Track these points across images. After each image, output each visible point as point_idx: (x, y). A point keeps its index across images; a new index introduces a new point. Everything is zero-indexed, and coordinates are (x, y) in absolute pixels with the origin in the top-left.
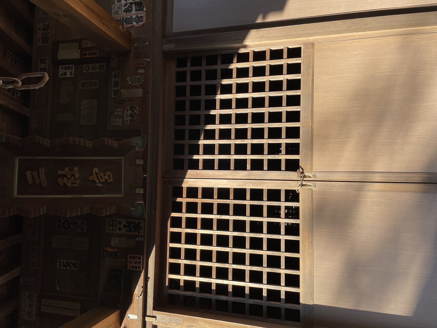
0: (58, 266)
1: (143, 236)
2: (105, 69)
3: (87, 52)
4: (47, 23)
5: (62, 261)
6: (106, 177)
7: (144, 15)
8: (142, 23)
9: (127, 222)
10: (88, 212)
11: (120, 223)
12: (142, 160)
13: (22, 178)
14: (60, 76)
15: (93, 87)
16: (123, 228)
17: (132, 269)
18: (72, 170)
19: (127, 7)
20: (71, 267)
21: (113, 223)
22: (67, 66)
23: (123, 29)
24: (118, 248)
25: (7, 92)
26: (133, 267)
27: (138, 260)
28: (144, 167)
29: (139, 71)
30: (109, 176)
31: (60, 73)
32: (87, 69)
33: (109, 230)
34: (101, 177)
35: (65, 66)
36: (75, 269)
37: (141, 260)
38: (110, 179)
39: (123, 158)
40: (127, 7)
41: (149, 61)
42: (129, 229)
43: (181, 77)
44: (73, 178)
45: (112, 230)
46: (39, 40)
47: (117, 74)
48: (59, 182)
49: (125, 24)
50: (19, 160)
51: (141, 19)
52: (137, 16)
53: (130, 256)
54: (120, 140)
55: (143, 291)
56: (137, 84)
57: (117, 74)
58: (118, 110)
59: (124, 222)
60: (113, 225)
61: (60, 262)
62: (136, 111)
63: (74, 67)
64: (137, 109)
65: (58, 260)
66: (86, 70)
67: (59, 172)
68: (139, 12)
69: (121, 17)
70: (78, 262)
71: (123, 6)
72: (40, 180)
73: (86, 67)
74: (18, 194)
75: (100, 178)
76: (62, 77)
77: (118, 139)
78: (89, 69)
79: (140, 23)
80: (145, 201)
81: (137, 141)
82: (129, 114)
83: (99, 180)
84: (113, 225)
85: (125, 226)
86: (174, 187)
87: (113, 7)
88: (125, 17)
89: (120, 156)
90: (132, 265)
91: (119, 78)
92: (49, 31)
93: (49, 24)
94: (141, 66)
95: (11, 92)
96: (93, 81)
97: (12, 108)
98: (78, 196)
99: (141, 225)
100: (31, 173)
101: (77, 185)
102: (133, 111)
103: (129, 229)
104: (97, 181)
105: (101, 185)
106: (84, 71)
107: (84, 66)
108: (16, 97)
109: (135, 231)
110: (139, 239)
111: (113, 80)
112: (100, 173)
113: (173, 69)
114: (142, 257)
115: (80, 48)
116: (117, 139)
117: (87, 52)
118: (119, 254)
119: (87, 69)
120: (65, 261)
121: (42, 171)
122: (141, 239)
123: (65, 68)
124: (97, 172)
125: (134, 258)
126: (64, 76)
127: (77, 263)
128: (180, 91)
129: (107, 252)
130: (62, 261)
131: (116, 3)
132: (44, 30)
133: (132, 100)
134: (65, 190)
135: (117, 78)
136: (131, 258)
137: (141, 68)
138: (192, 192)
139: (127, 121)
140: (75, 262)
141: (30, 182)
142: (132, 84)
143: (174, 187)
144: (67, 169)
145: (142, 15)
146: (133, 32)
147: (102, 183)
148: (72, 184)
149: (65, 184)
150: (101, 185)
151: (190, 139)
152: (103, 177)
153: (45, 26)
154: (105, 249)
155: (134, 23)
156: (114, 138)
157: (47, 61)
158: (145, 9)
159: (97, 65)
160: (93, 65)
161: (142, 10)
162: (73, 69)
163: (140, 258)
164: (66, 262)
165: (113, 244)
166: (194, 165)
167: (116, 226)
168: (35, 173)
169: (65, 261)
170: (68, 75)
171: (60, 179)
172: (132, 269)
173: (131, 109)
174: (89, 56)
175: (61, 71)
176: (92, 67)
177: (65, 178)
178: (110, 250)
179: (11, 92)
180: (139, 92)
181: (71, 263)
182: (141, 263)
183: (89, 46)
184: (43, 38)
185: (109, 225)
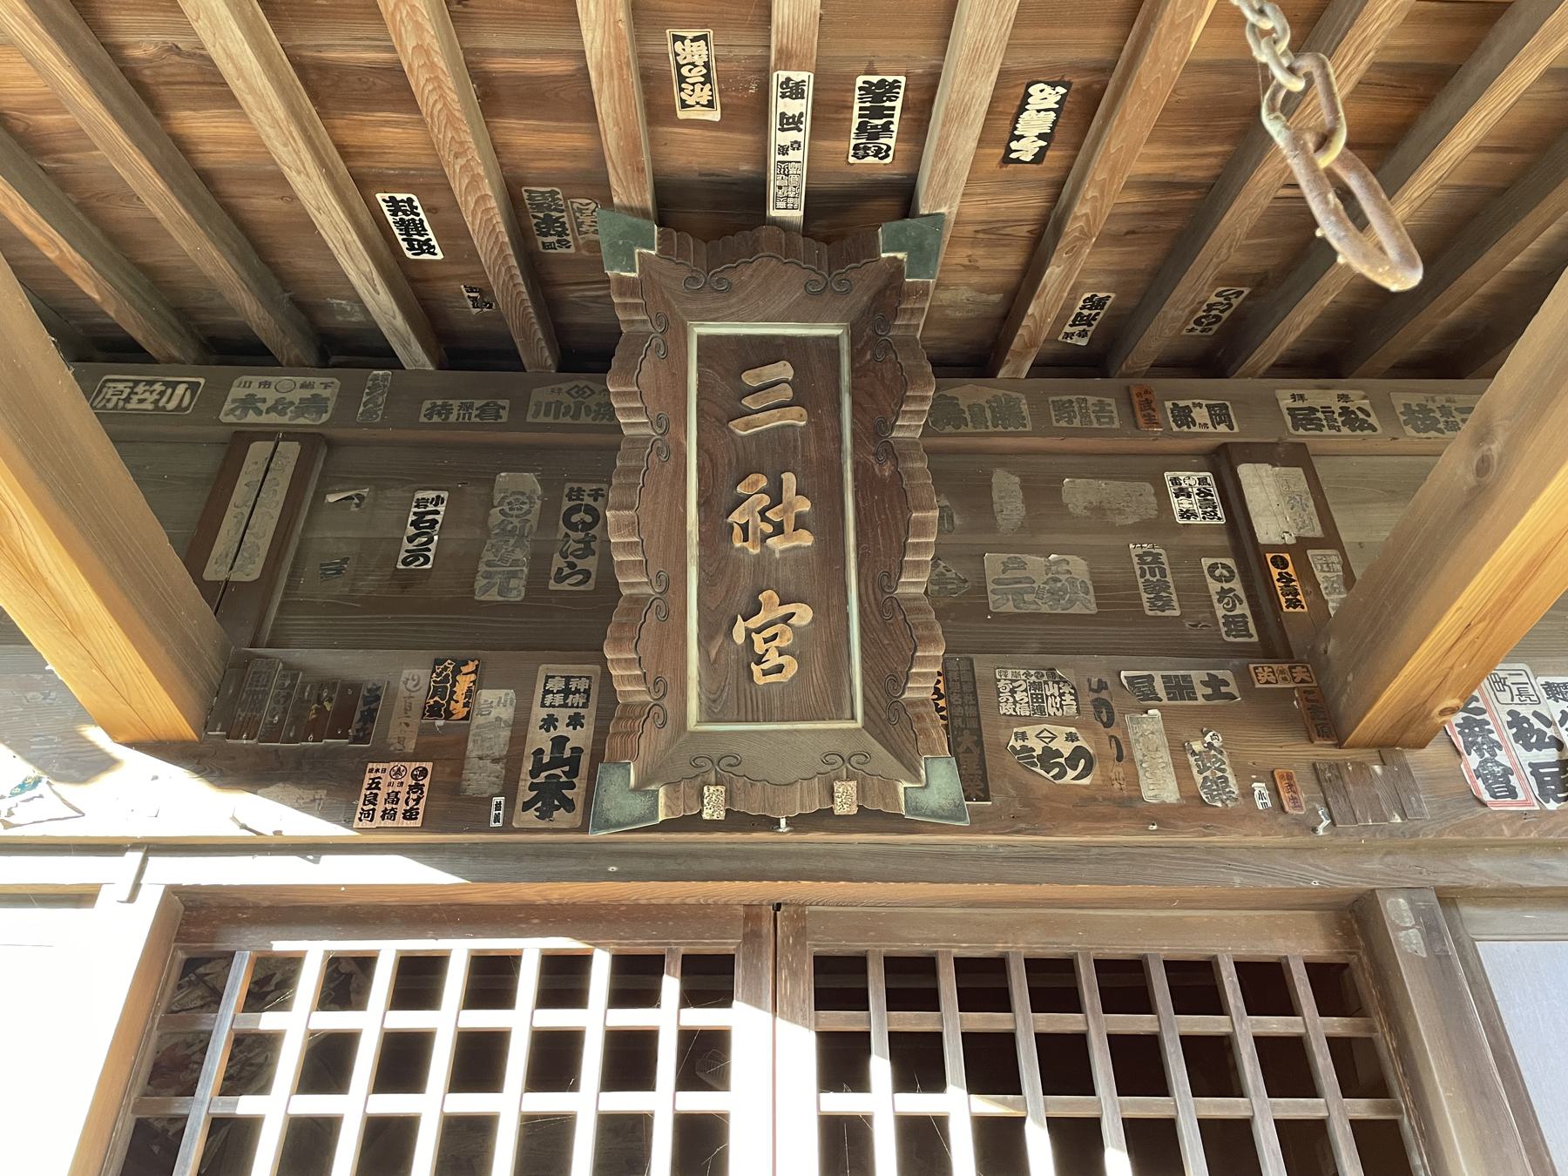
0: (419, 495)
1: (507, 828)
2: (1231, 639)
3: (1290, 569)
4: (1373, 420)
5: (441, 508)
6: (773, 659)
7: (1524, 803)
8: (1486, 797)
9: (577, 751)
10: (625, 592)
11: (575, 721)
12: (855, 810)
13: (769, 350)
14: (1168, 475)
15: (1145, 596)
16: (553, 733)
17: (367, 781)
18: (801, 522)
19: (1537, 724)
20: (411, 540)
21: (577, 691)
22: (1216, 499)
23: (1442, 713)
24: (466, 718)
25: (1088, 295)
26: (375, 784)
27: (401, 807)
28: (823, 819)
29: (1259, 787)
30: (779, 669)
31: (1182, 475)
32: (1217, 573)
33: (548, 678)
34: (774, 637)
35: (1214, 490)
36: (403, 555)
37: (400, 821)
38: (765, 673)
39: (859, 723)
40: (1537, 724)
41: (1314, 830)
42: (546, 759)
43: (1266, 985)
44: (769, 529)
45: (547, 692)
46: (1302, 397)
47: (1223, 689)
48: (753, 477)
49: (1458, 718)
50: (837, 339)
51: (1499, 788)
52: (1507, 772)
53: (424, 772)
54: (939, 710)
55: (262, 835)
56: (1199, 779)
57: (1223, 689)
58: (1068, 698)
59: (580, 737)
60: (567, 692)
61: (438, 500)
62: (1071, 774)
63: (1215, 522)
64: (1086, 781)
65: (445, 495)
66: (1213, 567)
67: (789, 480)
68: (1532, 780)
69: (1486, 702)
70: (429, 566)
71: (1537, 708)
72: (757, 412)
73: (1224, 566)
74: (704, 341)
75: (768, 633)
76: (1169, 484)
77: (942, 703)
78: (1219, 579)
79: (1480, 782)
80: (666, 826)
81: (940, 783)
82: (1054, 745)
83: (759, 631)
84: (567, 692)
85: (559, 742)
86: (730, 959)
87: (1517, 666)
88: (1486, 717)
89: (865, 713)
90: (385, 779)
91: (1206, 697)
92: (1345, 431)
93: (1375, 430)
94: (1285, 795)
95: (1086, 312)
96: (1174, 597)
97: (1030, 311)
98: (693, 551)
99: (560, 814)
100: (786, 381)
101: (738, 544)
102: (1072, 761)
103: (546, 759)
104: (755, 622)
105: (739, 635)
106: (1206, 562)
107: (1230, 562)
108: (1068, 329)
109: (532, 787)
110: (498, 806)
111: (1198, 676)
112: (789, 633)
113: (1299, 946)
114: (418, 823)
115: (1303, 544)
116: (941, 697)
117: (1290, 569)
118: (440, 723)
119: (1217, 573)
120: (439, 518)
121: (796, 418)
122: (497, 816)
123: (1203, 494)
124: (793, 621)
125: (417, 787)
126: (1171, 489)
127: (427, 560)
128: (1195, 985)
129: (457, 671)
130: (441, 508)
131: (1542, 680)
132: (1345, 411)
133: (1120, 758)
134: (716, 505)
135: (1209, 691)
136: (414, 777)
137: (1275, 792)
138: (705, 1059)
139: (1023, 736)
140: (431, 555)
141: (750, 378)
142: (1194, 753)
143: (730, 959)
144: (805, 506)
145: (1521, 796)
146: (1433, 752)
147: (749, 641)
148: (745, 528)
149: (741, 500)
150: (739, 635)
151: (966, 1036)
152: (776, 643)
153: (1361, 416)
154: (471, 667)
155: (1473, 760)
156: (941, 686)
157: (1222, 428)
158: (1552, 806)
159: (1243, 609)
160: (1241, 593)
161: (1545, 795)
162: (1208, 522)
163: (410, 815)
164: (435, 522)
165: (486, 695)
166: (842, 1063)
167: (565, 706)
168: (786, 393)
169: (439, 518)
170: (1178, 504)
171: (763, 483)
172: (367, 781)
173: (1078, 753)
174: (1276, 577)
175: (1190, 479)
176: (1231, 590)
177: (766, 500)
178: (464, 683)
179: (1086, 312)
180: (1160, 787)
181: (431, 540)
182: (388, 823)
183: (1319, 576)
184: (1313, 410)
185: (568, 679)
